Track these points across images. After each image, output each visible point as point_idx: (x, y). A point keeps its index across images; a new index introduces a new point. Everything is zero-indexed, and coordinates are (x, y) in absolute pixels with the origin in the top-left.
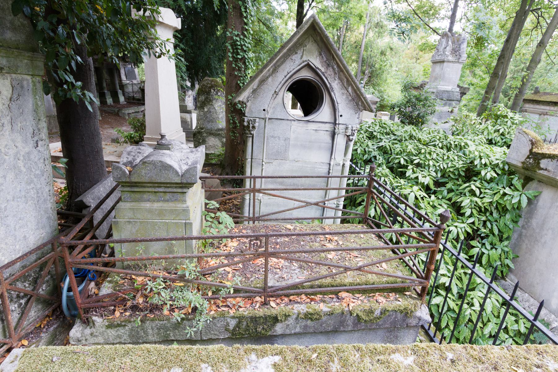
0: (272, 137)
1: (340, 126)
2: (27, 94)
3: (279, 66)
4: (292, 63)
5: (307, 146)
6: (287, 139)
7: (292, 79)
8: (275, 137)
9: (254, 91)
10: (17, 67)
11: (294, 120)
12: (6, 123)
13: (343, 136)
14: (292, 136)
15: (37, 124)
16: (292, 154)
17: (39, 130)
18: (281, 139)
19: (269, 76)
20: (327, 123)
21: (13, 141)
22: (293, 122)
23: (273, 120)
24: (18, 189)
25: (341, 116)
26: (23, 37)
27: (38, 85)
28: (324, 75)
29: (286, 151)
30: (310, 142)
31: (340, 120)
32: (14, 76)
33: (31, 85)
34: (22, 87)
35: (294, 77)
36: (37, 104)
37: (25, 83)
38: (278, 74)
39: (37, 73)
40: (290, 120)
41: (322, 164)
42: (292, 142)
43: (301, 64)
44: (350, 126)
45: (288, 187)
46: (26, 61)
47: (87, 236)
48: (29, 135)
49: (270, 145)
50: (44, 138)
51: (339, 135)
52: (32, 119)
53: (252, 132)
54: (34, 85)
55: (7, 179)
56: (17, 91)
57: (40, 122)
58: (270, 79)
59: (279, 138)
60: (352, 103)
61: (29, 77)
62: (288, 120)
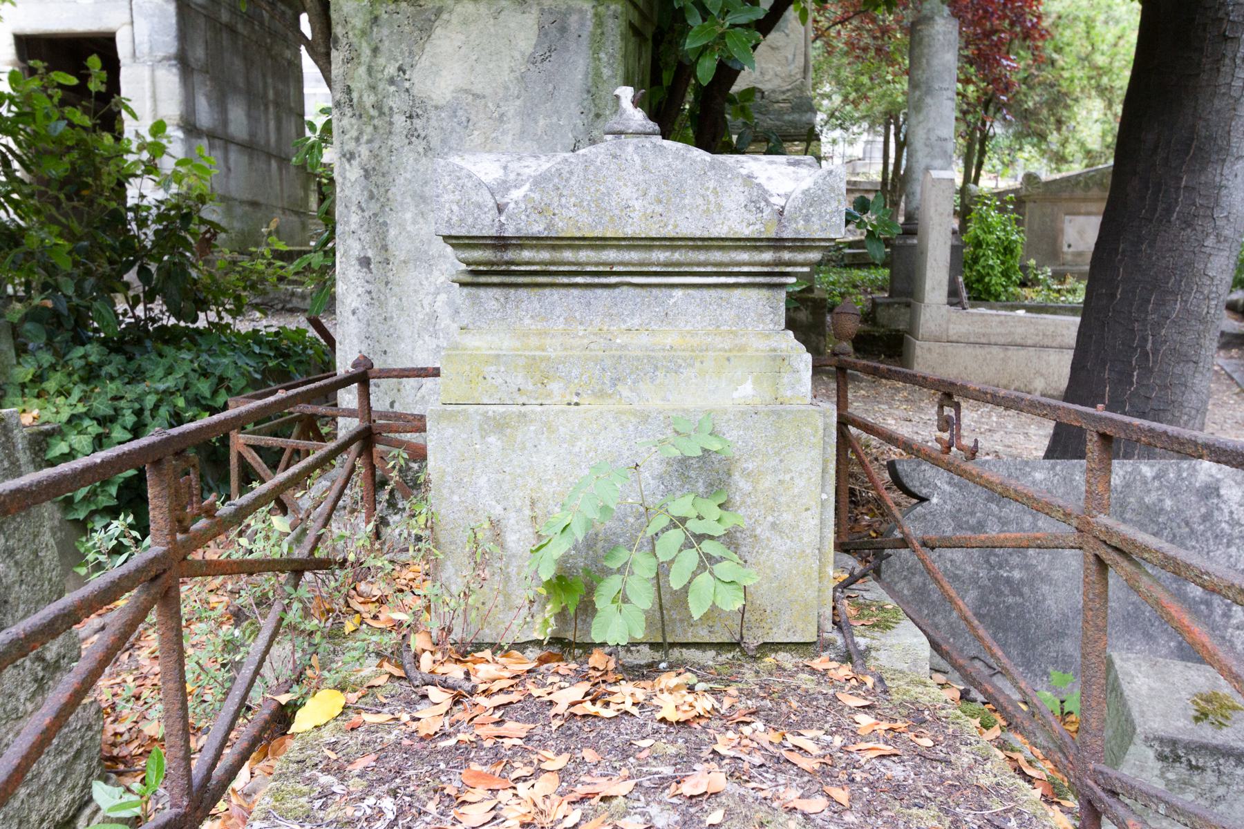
34: (563, 30)
36: (598, 74)
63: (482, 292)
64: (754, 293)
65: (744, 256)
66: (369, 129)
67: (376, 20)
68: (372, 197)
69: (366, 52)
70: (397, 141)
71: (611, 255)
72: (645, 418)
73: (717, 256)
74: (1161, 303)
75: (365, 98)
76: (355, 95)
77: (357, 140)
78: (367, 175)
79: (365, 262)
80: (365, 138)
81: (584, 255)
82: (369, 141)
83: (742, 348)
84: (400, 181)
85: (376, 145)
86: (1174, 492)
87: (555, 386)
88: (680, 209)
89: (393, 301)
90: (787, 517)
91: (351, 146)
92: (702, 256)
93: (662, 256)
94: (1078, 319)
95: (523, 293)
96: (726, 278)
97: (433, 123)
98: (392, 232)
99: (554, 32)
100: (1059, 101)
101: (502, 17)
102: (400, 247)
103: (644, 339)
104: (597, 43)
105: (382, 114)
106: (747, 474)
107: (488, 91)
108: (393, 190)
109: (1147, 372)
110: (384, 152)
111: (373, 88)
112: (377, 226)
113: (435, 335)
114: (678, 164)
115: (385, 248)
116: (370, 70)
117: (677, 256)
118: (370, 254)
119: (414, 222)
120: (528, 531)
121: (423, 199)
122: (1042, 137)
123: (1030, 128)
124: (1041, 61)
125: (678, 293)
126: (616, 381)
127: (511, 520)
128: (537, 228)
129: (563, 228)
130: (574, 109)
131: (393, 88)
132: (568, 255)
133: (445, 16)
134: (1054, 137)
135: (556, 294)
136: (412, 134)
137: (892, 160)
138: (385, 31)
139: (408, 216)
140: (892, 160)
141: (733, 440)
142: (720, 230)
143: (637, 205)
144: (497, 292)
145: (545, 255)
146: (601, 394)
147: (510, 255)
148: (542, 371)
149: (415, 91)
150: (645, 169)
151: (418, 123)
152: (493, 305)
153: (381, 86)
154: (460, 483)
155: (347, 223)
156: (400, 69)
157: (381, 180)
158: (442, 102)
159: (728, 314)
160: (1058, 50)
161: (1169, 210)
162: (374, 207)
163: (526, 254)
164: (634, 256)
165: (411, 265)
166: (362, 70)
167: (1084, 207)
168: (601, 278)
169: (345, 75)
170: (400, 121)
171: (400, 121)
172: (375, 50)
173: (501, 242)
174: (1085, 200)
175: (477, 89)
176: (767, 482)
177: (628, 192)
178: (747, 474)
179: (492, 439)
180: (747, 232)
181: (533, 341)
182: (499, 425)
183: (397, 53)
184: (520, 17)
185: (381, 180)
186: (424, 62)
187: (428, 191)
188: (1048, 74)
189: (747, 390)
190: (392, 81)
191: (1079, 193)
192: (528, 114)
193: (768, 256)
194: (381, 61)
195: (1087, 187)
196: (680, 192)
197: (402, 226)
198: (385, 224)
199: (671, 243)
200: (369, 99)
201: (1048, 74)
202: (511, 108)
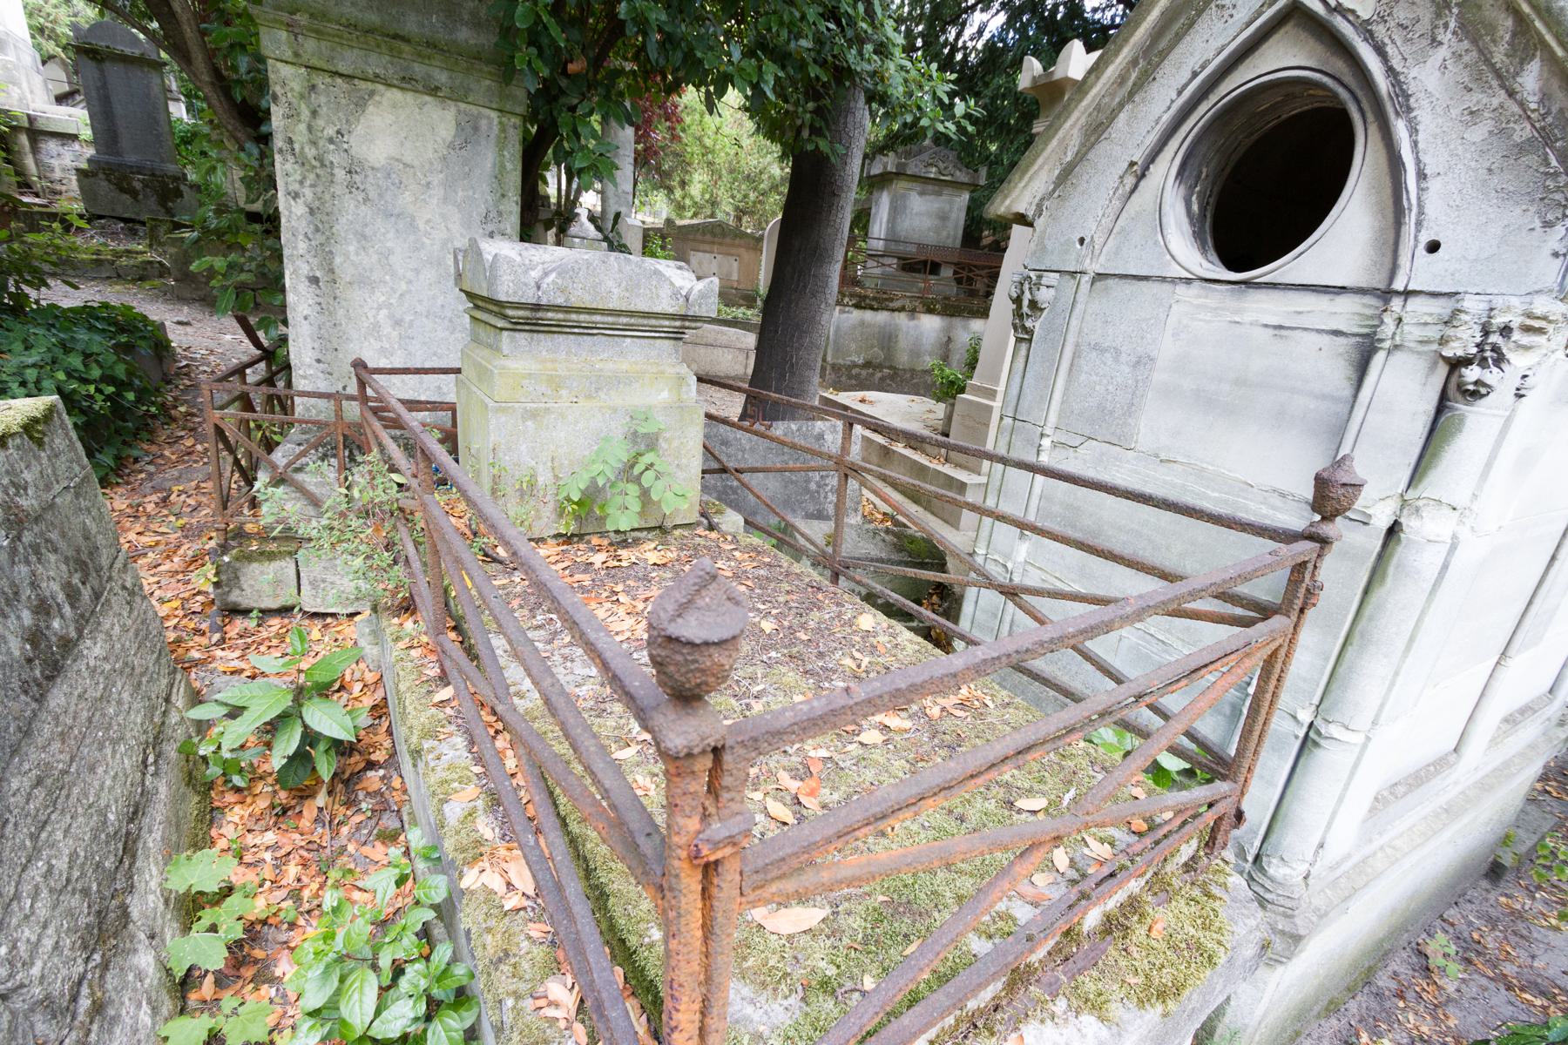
0: (1096, 347)
1: (1414, 304)
2: (483, 143)
3: (1164, 55)
4: (1220, 25)
5: (1225, 398)
6: (1143, 362)
7: (1213, 98)
8: (1104, 351)
9: (1066, 174)
10: (468, 90)
11: (1188, 281)
12: (435, 183)
13: (1422, 365)
14: (1167, 349)
15: (497, 203)
16: (1155, 426)
17: (500, 214)
18: (1124, 358)
19: (1121, 105)
20: (1343, 289)
21: (443, 216)
22: (1181, 289)
23: (1110, 282)
24: (439, 303)
25: (1433, 247)
26: (494, 39)
27: (511, 131)
28: (1369, 36)
29: (1131, 409)
30: (1241, 382)
31: (1418, 271)
32: (462, 106)
33: (496, 129)
34: (476, 129)
35: (1224, 88)
36: (503, 166)
37: (483, 122)
38: (1155, 86)
39: (508, 107)
40: (1174, 281)
41: (1277, 501)
42: (1159, 377)
43: (1259, 14)
44: (1474, 306)
45: (1396, 689)
46: (488, 82)
47: (1425, 851)
48: (477, 218)
49: (1083, 377)
50: (509, 231)
51: (1398, 356)
52: (488, 189)
53: (1028, 324)
54: (503, 129)
55: (422, 277)
56: (468, 133)
57: (505, 201)
58: (1123, 117)
59: (1118, 352)
60: (1532, 160)
61: (494, 115)
62: (1163, 279)
63: (517, 335)
64: (667, 342)
65: (667, 323)
66: (312, 176)
67: (313, 87)
68: (317, 230)
69: (305, 113)
70: (338, 189)
71: (598, 318)
72: (615, 410)
73: (653, 322)
74: (800, 337)
75: (306, 150)
76: (297, 146)
77: (301, 183)
78: (312, 212)
79: (314, 280)
80: (308, 183)
81: (582, 317)
82: (312, 186)
83: (663, 372)
84: (343, 220)
85: (319, 189)
86: (805, 437)
87: (564, 392)
88: (638, 296)
89: (341, 312)
90: (684, 461)
91: (296, 187)
92: (645, 322)
93: (624, 320)
94: (751, 340)
95: (542, 336)
96: (655, 334)
97: (371, 179)
98: (338, 260)
99: (469, 130)
100: (684, 164)
101: (426, 109)
102: (345, 272)
103: (611, 366)
104: (501, 144)
105: (323, 165)
106: (666, 440)
107: (416, 163)
108: (337, 227)
109: (793, 374)
110: (327, 197)
111: (314, 143)
112: (324, 253)
113: (379, 339)
114: (637, 270)
115: (332, 271)
116: (310, 128)
117: (633, 321)
118: (318, 274)
119: (357, 254)
120: (550, 475)
121: (364, 237)
122: (670, 190)
123: (663, 181)
124: (675, 138)
125: (628, 340)
126: (597, 390)
127: (541, 468)
128: (560, 301)
129: (574, 301)
130: (486, 188)
131: (332, 147)
132: (574, 317)
133: (377, 98)
134: (678, 193)
135: (561, 338)
136: (351, 186)
137: (564, 187)
138: (323, 99)
139: (351, 248)
140: (564, 187)
141: (659, 422)
142: (658, 309)
143: (615, 291)
144: (526, 335)
145: (561, 316)
146: (589, 397)
147: (540, 314)
148: (556, 383)
149: (353, 152)
150: (620, 271)
151: (357, 178)
152: (523, 342)
153: (321, 143)
154: (509, 449)
155: (295, 248)
156: (338, 132)
157: (325, 218)
158: (377, 165)
159: (654, 353)
160: (684, 130)
161: (805, 287)
162: (320, 238)
163: (550, 315)
164: (610, 319)
165: (356, 286)
166: (302, 127)
167: (702, 247)
168: (587, 330)
169: (286, 128)
170: (340, 174)
171: (340, 174)
172: (314, 113)
173: (537, 307)
174: (703, 242)
175: (408, 159)
176: (676, 443)
177: (610, 283)
178: (666, 440)
179: (529, 423)
180: (671, 311)
181: (549, 365)
182: (533, 415)
183: (334, 118)
184: (441, 112)
185: (325, 218)
186: (359, 129)
187: (368, 231)
188: (676, 147)
189: (665, 395)
190: (331, 141)
191: (699, 237)
192: (449, 185)
193: (678, 323)
194: (320, 122)
195: (704, 234)
196: (638, 286)
197: (346, 255)
198: (331, 252)
199: (631, 314)
200: (310, 152)
201: (676, 147)
202: (436, 179)
